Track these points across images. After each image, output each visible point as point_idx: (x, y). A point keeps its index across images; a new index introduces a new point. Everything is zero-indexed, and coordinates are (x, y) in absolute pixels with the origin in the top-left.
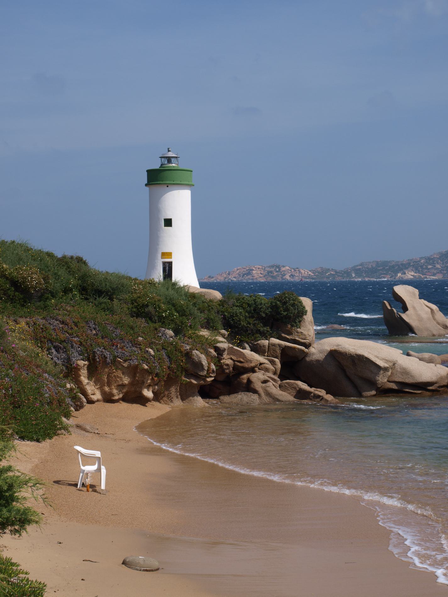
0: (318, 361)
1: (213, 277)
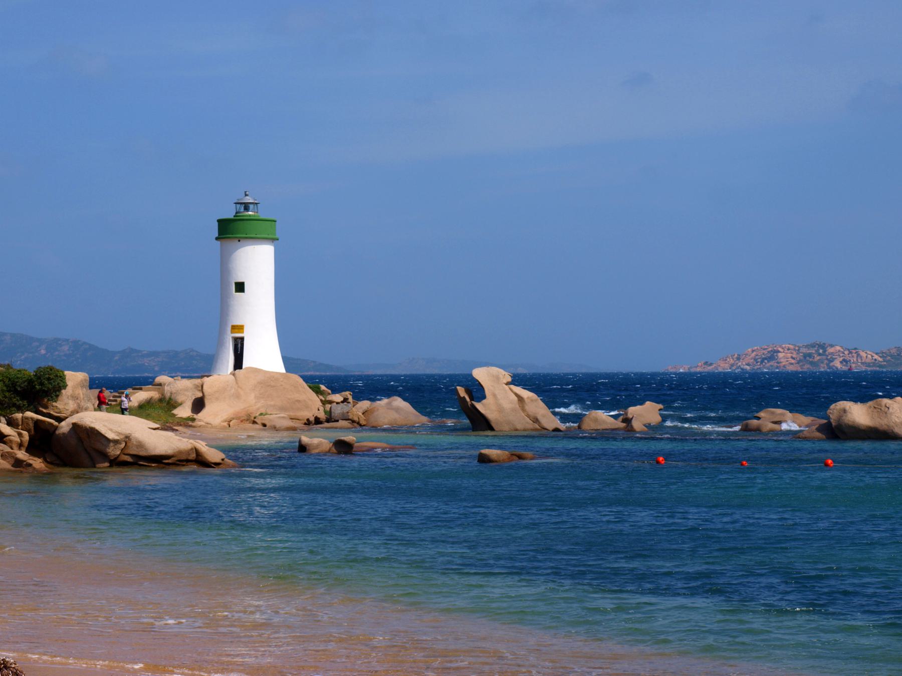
0: (64, 434)
1: (711, 364)
